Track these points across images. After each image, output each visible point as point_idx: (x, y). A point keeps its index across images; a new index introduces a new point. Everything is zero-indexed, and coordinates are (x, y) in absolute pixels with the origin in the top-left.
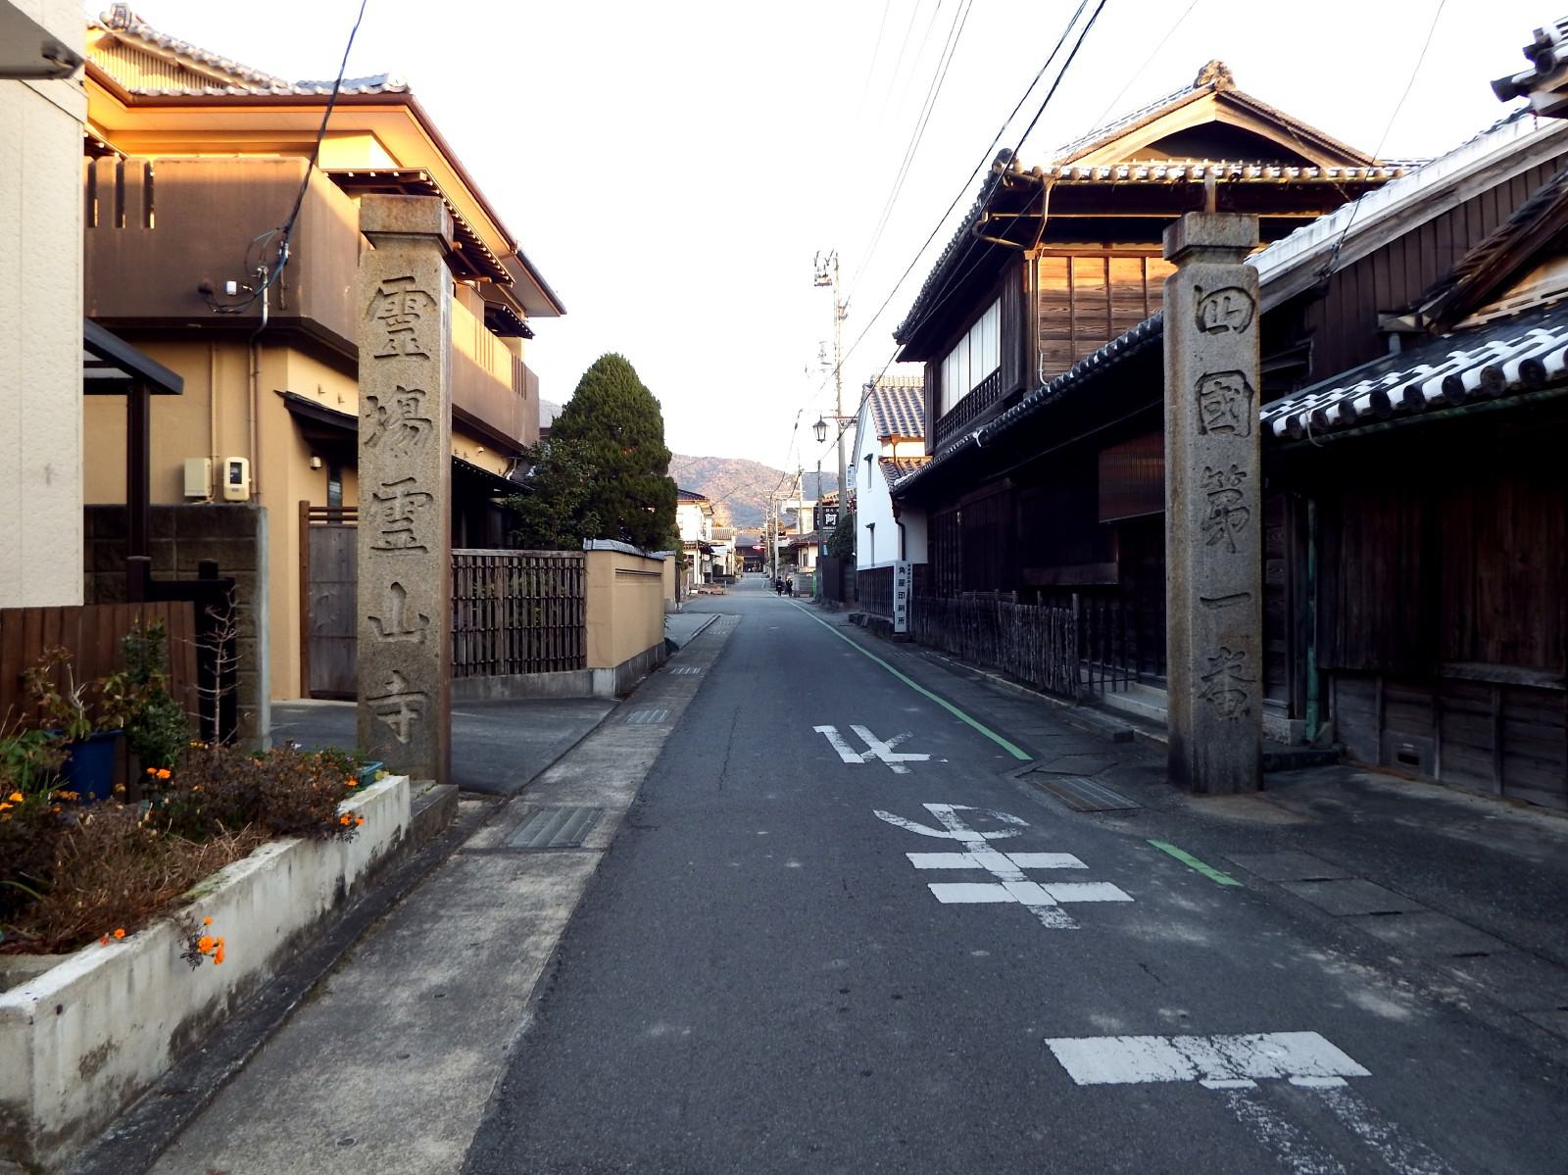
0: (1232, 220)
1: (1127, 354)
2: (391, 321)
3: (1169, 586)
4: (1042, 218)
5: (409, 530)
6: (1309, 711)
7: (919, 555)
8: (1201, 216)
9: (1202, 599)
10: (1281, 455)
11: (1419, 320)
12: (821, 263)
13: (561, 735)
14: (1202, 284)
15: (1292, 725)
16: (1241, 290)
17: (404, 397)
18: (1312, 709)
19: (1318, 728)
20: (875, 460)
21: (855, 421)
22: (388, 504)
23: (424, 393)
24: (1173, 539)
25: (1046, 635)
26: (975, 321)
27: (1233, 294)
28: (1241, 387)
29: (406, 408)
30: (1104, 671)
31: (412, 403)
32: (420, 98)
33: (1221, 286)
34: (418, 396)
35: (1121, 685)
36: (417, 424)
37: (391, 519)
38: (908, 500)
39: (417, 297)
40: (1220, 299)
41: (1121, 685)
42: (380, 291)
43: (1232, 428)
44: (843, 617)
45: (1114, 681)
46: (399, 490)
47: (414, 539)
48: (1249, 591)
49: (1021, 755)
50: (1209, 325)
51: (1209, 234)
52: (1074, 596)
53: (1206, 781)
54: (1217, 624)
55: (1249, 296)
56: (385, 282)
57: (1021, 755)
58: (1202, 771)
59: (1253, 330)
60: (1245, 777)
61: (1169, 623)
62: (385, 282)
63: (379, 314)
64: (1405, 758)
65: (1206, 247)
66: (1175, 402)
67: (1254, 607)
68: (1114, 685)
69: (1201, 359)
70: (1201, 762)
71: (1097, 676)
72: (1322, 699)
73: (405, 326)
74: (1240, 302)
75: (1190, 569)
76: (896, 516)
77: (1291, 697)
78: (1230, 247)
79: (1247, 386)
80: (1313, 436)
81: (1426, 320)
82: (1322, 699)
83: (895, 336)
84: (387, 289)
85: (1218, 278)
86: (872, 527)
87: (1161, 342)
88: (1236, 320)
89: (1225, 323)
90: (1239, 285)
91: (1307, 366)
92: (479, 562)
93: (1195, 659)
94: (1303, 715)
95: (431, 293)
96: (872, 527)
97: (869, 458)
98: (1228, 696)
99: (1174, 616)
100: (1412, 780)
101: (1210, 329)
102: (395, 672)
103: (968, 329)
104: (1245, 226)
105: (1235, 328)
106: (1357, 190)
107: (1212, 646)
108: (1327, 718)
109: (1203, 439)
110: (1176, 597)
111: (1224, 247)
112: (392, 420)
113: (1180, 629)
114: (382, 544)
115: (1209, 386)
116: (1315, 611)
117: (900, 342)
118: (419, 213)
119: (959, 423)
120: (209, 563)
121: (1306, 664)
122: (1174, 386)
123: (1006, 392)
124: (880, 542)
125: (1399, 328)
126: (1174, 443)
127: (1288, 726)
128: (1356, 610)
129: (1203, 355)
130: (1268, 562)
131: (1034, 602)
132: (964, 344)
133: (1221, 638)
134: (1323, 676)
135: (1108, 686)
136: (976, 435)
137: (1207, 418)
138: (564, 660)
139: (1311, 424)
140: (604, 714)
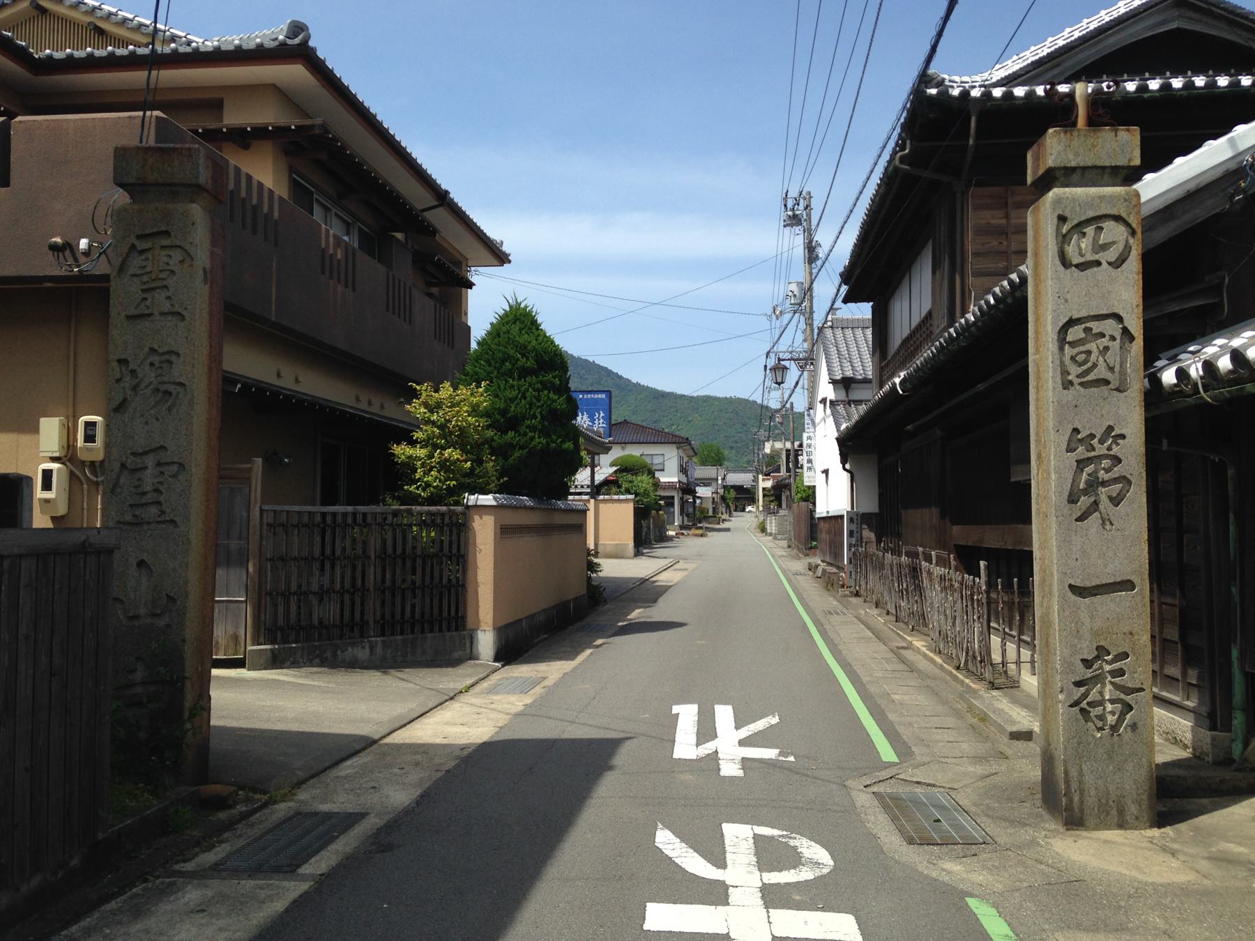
0: (1106, 133)
2: (145, 279)
5: (159, 503)
6: (1235, 722)
7: (870, 505)
8: (1065, 132)
9: (1071, 586)
12: (790, 204)
14: (1067, 214)
15: (1213, 739)
16: (1118, 218)
17: (155, 359)
22: (138, 475)
23: (178, 355)
27: (1108, 225)
29: (159, 371)
31: (165, 366)
33: (1091, 214)
34: (173, 358)
36: (171, 388)
37: (140, 490)
40: (1090, 230)
42: (133, 246)
43: (1107, 382)
44: (800, 565)
46: (150, 461)
47: (163, 512)
48: (1133, 578)
49: (887, 753)
51: (1077, 154)
52: (982, 563)
53: (1082, 811)
54: (1092, 617)
55: (1127, 224)
56: (139, 237)
57: (887, 753)
58: (1076, 799)
59: (1134, 264)
60: (1133, 809)
62: (139, 237)
63: (132, 270)
65: (1074, 169)
66: (1037, 351)
67: (1139, 598)
69: (1066, 301)
70: (1074, 786)
73: (159, 284)
74: (1114, 232)
75: (1055, 550)
76: (844, 462)
78: (1103, 168)
79: (1125, 331)
80: (1205, 391)
84: (141, 245)
85: (1089, 203)
86: (826, 472)
88: (1112, 254)
89: (1096, 257)
90: (1114, 212)
92: (329, 519)
93: (1063, 660)
94: (1227, 727)
95: (188, 247)
96: (826, 472)
98: (1109, 707)
101: (1077, 266)
102: (138, 658)
104: (1125, 144)
105: (1109, 264)
107: (1085, 644)
109: (1069, 395)
110: (1043, 581)
111: (1095, 167)
112: (143, 386)
113: (1047, 623)
114: (128, 518)
115: (1075, 333)
116: (1237, 600)
122: (1037, 332)
127: (1209, 740)
129: (1068, 296)
130: (1186, 536)
133: (1096, 634)
136: (897, 380)
138: (441, 622)
139: (1202, 378)
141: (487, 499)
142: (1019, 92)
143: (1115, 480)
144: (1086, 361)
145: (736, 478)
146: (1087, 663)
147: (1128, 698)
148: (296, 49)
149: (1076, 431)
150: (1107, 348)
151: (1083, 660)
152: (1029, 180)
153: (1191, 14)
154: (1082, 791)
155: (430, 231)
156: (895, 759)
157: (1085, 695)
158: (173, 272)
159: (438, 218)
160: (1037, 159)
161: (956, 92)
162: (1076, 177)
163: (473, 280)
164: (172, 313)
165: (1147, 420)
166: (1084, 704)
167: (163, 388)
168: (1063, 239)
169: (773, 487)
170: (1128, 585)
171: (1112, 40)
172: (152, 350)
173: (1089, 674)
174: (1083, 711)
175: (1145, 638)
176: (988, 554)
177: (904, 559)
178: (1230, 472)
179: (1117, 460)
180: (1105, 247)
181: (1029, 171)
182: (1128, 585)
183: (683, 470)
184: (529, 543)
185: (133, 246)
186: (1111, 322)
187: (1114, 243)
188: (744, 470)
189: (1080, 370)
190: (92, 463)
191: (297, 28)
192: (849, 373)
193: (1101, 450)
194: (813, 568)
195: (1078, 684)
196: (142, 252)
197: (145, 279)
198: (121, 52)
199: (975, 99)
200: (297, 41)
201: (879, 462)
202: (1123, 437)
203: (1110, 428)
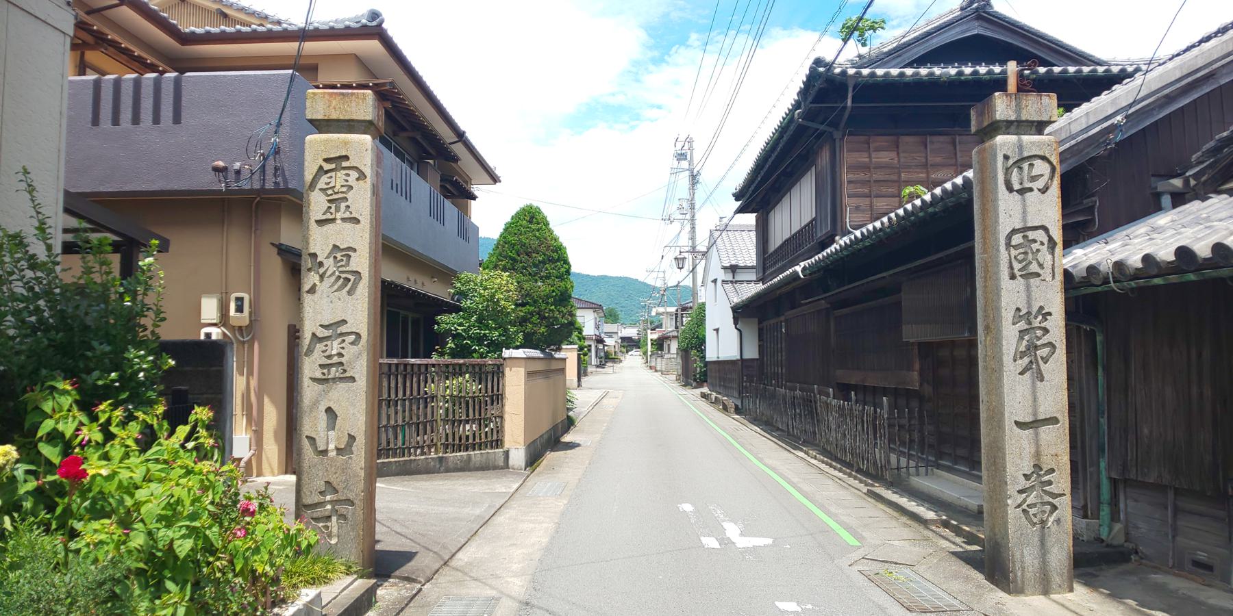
1: (931, 210)
2: (330, 192)
3: (982, 407)
4: (845, 108)
10: (1088, 301)
11: (1186, 182)
13: (478, 511)
16: (1043, 158)
18: (1105, 511)
19: (1111, 530)
20: (719, 282)
21: (704, 254)
23: (355, 250)
24: (986, 368)
25: (859, 427)
26: (793, 185)
27: (1037, 162)
28: (1045, 240)
30: (910, 457)
32: (390, 28)
35: (922, 470)
37: (327, 354)
38: (741, 312)
39: (350, 172)
40: (1026, 166)
41: (922, 470)
42: (321, 167)
43: (1038, 275)
45: (917, 467)
50: (1016, 186)
61: (984, 441)
62: (326, 160)
64: (1198, 564)
68: (917, 470)
71: (903, 461)
72: (1114, 502)
74: (1041, 168)
76: (736, 323)
77: (1086, 499)
78: (1033, 122)
79: (1051, 239)
81: (1193, 182)
82: (1114, 502)
83: (734, 195)
84: (327, 167)
87: (970, 201)
88: (1040, 184)
91: (1093, 219)
96: (717, 330)
97: (715, 281)
99: (989, 435)
100: (1209, 586)
103: (789, 190)
106: (1121, 77)
108: (1118, 520)
110: (990, 419)
115: (1017, 240)
117: (737, 200)
118: (354, 104)
119: (782, 259)
120: (180, 391)
121: (1099, 472)
123: (821, 233)
124: (724, 343)
125: (1171, 189)
126: (985, 287)
128: (1146, 431)
131: (848, 399)
132: (786, 200)
134: (1114, 482)
135: (912, 471)
137: (1017, 266)
140: (515, 486)
141: (520, 353)
142: (865, 72)
143: (1045, 345)
144: (1024, 260)
145: (632, 332)
146: (1027, 477)
147: (1055, 501)
148: (373, 30)
149: (1018, 309)
150: (1038, 250)
151: (1024, 475)
152: (973, 129)
153: (986, 25)
154: (1023, 568)
155: (455, 159)
156: (858, 544)
157: (1025, 501)
158: (351, 188)
159: (458, 149)
160: (981, 114)
161: (837, 71)
162: (1013, 128)
163: (476, 193)
164: (350, 219)
165: (1066, 299)
166: (1024, 506)
167: (344, 276)
168: (1008, 171)
169: (659, 339)
170: (1053, 420)
171: (935, 41)
172: (335, 247)
173: (1028, 484)
174: (1024, 510)
175: (1066, 459)
176: (855, 388)
177: (798, 392)
178: (1099, 338)
179: (1046, 331)
180: (1034, 179)
181: (973, 123)
182: (1053, 420)
183: (597, 327)
184: (540, 382)
185: (321, 167)
186: (1041, 232)
187: (1042, 175)
188: (633, 325)
189: (1020, 266)
190: (240, 328)
191: (375, 15)
192: (734, 263)
193: (1036, 323)
194: (704, 396)
195: (1020, 492)
196: (327, 172)
197: (330, 192)
198: (245, 29)
199: (851, 76)
200: (374, 23)
201: (760, 323)
202: (1050, 314)
203: (1041, 308)
